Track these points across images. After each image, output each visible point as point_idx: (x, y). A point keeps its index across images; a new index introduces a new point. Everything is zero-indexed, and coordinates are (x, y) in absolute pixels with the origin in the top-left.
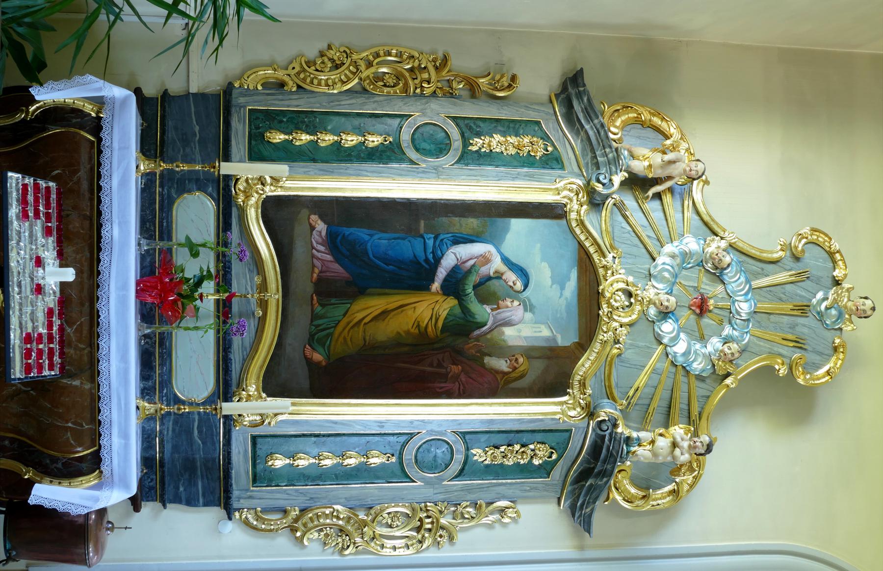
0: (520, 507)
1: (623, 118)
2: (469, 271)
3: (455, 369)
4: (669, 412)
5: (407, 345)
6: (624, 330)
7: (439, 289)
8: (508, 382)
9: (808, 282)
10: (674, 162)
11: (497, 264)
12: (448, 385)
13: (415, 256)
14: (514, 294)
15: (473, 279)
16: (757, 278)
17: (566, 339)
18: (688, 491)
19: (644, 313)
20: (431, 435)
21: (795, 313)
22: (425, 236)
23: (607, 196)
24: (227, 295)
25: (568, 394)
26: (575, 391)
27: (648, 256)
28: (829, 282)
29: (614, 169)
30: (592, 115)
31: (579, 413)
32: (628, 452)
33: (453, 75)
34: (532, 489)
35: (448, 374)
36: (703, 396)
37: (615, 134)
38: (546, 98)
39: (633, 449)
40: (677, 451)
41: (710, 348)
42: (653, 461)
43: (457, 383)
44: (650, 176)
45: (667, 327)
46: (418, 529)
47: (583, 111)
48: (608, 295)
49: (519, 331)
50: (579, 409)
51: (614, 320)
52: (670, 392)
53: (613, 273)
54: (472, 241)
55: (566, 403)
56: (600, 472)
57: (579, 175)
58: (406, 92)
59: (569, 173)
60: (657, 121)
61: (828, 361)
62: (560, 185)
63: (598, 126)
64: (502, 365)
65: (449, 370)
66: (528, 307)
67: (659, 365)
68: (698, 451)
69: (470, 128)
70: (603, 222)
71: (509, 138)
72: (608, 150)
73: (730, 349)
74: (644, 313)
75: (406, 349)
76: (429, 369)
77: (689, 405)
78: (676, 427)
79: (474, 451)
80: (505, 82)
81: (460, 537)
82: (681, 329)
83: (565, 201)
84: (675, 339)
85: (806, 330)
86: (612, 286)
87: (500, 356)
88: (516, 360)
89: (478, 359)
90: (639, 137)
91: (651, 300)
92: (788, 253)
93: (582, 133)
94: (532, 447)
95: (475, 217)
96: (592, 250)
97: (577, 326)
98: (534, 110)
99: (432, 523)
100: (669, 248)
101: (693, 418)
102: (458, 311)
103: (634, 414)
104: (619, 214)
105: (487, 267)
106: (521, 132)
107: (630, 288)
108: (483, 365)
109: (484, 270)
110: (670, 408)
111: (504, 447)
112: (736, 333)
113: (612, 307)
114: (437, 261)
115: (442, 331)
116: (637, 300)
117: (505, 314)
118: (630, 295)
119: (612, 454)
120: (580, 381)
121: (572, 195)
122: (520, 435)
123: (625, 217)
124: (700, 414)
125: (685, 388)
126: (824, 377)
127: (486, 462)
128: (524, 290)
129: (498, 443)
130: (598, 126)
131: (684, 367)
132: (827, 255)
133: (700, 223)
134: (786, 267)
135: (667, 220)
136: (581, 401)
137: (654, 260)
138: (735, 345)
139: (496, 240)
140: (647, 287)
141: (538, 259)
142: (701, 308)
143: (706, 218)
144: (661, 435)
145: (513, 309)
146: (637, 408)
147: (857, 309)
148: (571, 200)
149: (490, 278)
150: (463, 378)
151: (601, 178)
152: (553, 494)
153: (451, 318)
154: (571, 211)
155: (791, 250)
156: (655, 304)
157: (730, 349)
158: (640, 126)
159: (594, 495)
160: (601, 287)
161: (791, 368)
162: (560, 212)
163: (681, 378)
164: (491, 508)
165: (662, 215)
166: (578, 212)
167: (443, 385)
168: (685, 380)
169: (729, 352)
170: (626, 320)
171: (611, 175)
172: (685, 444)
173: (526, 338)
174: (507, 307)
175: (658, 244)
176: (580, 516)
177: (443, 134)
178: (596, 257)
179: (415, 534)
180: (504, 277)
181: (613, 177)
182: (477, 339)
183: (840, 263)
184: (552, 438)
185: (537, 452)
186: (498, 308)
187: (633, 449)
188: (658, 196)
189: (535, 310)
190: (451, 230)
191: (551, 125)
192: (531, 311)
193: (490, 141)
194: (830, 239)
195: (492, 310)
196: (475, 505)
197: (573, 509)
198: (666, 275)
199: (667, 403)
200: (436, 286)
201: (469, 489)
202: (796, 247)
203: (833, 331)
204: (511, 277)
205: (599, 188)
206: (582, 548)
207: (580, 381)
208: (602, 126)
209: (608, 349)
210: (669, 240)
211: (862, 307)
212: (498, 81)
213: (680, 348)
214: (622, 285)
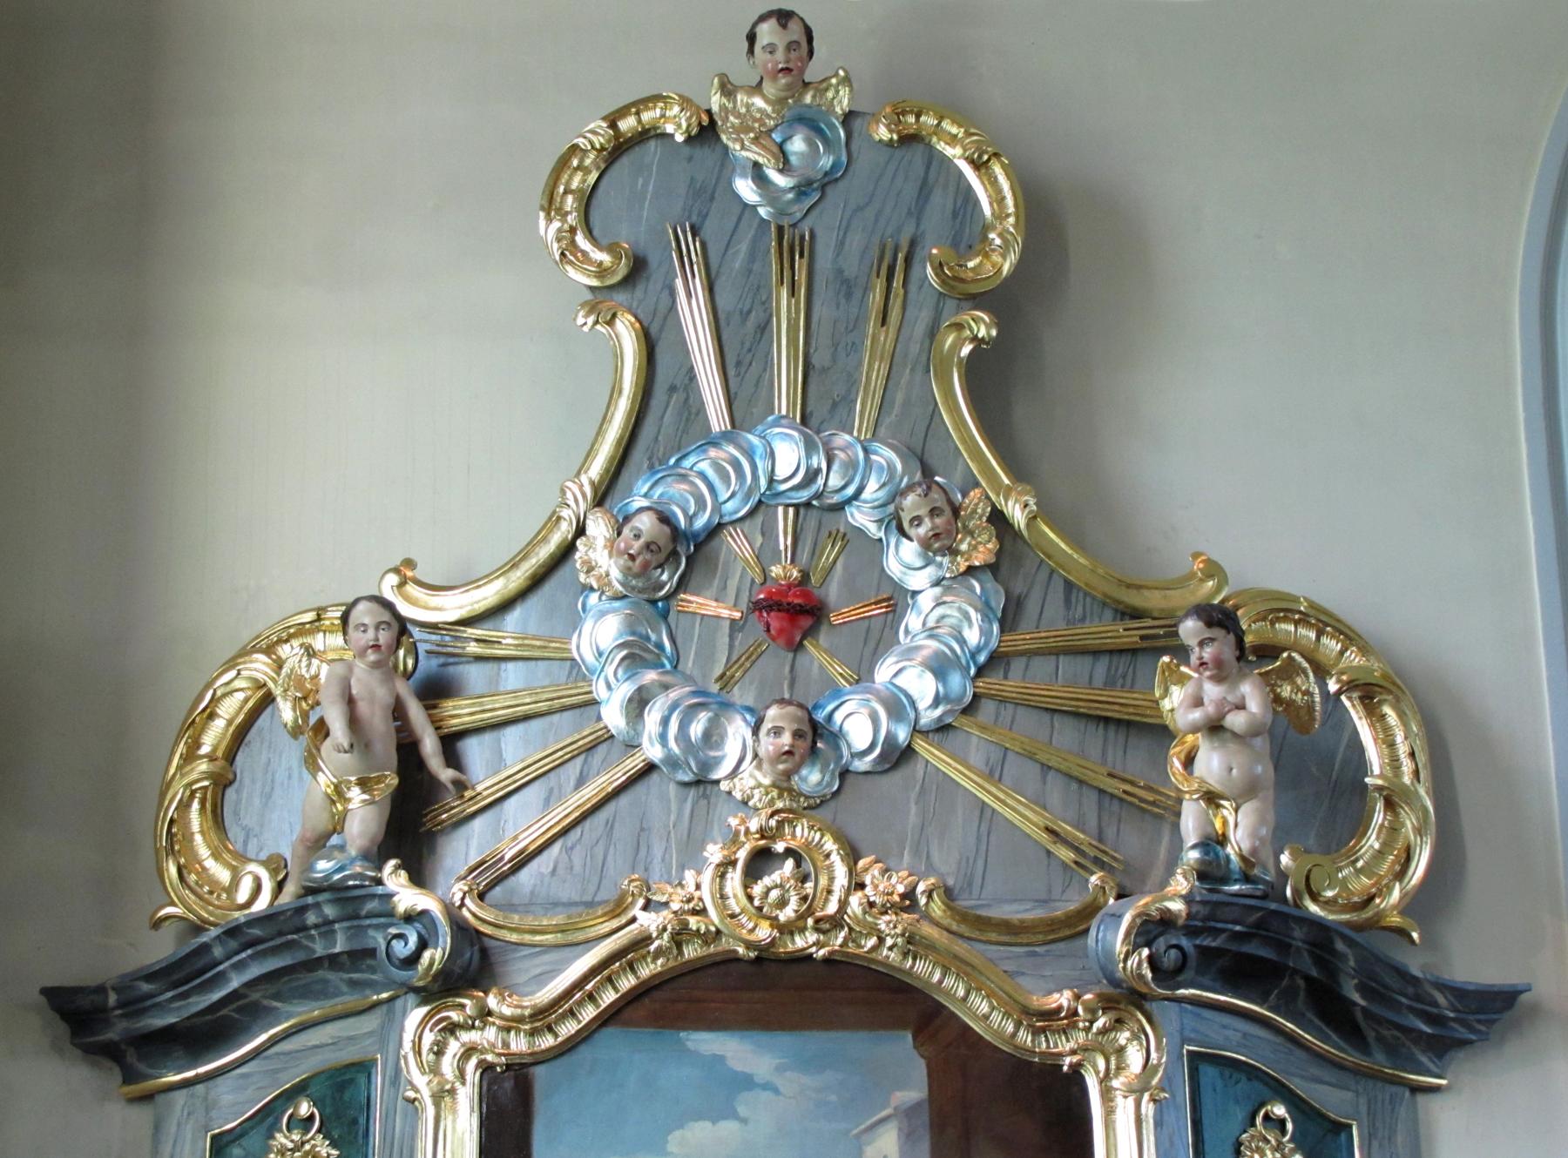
1: (204, 852)
4: (1119, 722)
9: (708, 231)
10: (350, 702)
16: (701, 409)
18: (1364, 650)
19: (815, 805)
21: (801, 277)
25: (1076, 1069)
27: (639, 789)
28: (704, 154)
29: (371, 906)
30: (200, 964)
31: (1135, 1037)
32: (1247, 878)
36: (1067, 601)
37: (258, 889)
40: (1236, 721)
41: (918, 580)
42: (1271, 793)
44: (393, 781)
45: (858, 726)
48: (764, 932)
50: (1123, 1037)
52: (1056, 717)
53: (695, 912)
55: (1105, 1080)
56: (1320, 962)
57: (391, 1012)
59: (383, 1048)
60: (214, 736)
61: (946, 162)
62: (422, 1083)
67: (976, 758)
68: (1229, 653)
72: (311, 918)
74: (815, 805)
77: (1096, 653)
78: (1166, 704)
82: (862, 676)
84: (897, 705)
85: (855, 241)
92: (621, 297)
93: (255, 996)
96: (627, 983)
97: (862, 1035)
101: (1132, 639)
103: (1130, 841)
104: (512, 880)
107: (742, 855)
110: (1107, 720)
112: (872, 490)
113: (801, 917)
118: (761, 861)
119: (1259, 925)
120: (1037, 1032)
121: (454, 1047)
123: (523, 860)
125: (1042, 666)
126: (994, 182)
131: (981, 671)
133: (535, 601)
134: (663, 308)
135: (526, 718)
136: (1099, 1024)
138: (910, 500)
140: (738, 795)
142: (795, 613)
143: (517, 579)
144: (1189, 762)
146: (1110, 832)
147: (787, 70)
148: (469, 1051)
151: (402, 950)
152: (1402, 1112)
155: (611, 287)
156: (788, 775)
157: (917, 521)
158: (230, 793)
159: (1391, 980)
162: (508, 1085)
163: (1011, 683)
165: (511, 733)
168: (1018, 665)
171: (390, 914)
172: (1212, 691)
175: (602, 749)
178: (646, 971)
181: (401, 909)
183: (647, 116)
188: (450, 743)
194: (575, 147)
198: (696, 729)
199: (1091, 727)
202: (602, 272)
203: (854, 147)
205: (434, 957)
207: (1037, 1032)
209: (927, 930)
210: (590, 710)
211: (780, 55)
213: (922, 687)
214: (735, 878)
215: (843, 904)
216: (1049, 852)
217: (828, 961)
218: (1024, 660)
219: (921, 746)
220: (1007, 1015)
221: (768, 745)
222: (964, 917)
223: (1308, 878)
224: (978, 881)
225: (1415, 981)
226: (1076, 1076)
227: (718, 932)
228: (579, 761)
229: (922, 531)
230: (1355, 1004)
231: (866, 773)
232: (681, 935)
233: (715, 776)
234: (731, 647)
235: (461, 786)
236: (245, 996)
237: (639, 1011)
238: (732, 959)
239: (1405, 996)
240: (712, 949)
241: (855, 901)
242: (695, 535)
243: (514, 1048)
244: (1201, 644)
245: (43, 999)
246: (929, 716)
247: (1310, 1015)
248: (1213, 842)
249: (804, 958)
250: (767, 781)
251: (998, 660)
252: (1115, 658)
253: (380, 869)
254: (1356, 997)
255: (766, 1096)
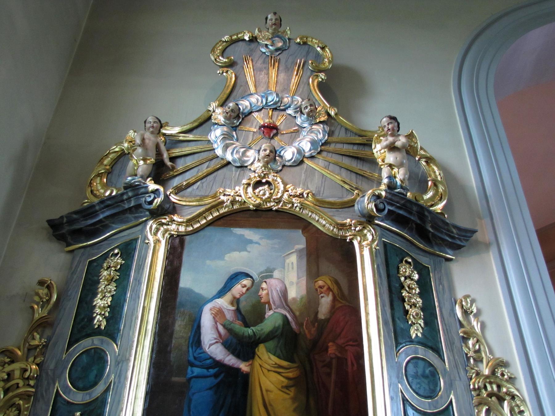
0: (460, 294)
2: (230, 330)
3: (332, 349)
5: (308, 401)
6: (290, 187)
7: (247, 364)
8: (343, 296)
11: (223, 303)
12: (350, 357)
13: (210, 389)
14: (255, 287)
15: (238, 327)
17: (300, 241)
20: (402, 378)
22: (189, 375)
23: (167, 197)
24: (313, 127)
25: (351, 240)
26: (349, 235)
27: (225, 170)
30: (91, 211)
33: (24, 344)
34: (441, 283)
35: (338, 358)
36: (346, 133)
38: (69, 257)
39: (399, 183)
43: (347, 348)
45: (289, 154)
46: (501, 400)
47: (86, 220)
48: (258, 201)
49: (292, 283)
50: (365, 231)
51: (281, 197)
53: (238, 196)
54: (199, 327)
55: (360, 243)
56: (420, 219)
58: (29, 396)
62: (151, 238)
63: (102, 206)
64: (326, 301)
65: (333, 356)
66: (268, 274)
69: (83, 327)
70: (191, 204)
71: (100, 290)
73: (306, 107)
75: (312, 403)
76: (333, 377)
78: (374, 151)
79: (414, 336)
80: (43, 291)
81: (499, 354)
83: (167, 235)
86: (251, 198)
87: (317, 304)
88: (321, 287)
89: (322, 326)
90: (119, 176)
91: (264, 166)
93: (107, 222)
94: (402, 279)
95: (173, 324)
96: (216, 214)
98: (77, 266)
99: (491, 383)
100: (219, 152)
102: (271, 344)
104: (184, 192)
105: (226, 313)
106: (96, 278)
107: (252, 182)
108: (327, 320)
109: (229, 316)
111: (406, 305)
114: (218, 364)
115: (291, 360)
116: (264, 177)
117: (275, 296)
118: (258, 184)
119: (404, 205)
120: (339, 230)
121: (162, 229)
122: (393, 289)
124: (360, 136)
127: (422, 325)
128: (251, 277)
129: (402, 312)
130: (102, 206)
132: (233, 45)
137: (229, 163)
139: (199, 304)
141: (220, 263)
142: (270, 130)
143: (196, 124)
144: (383, 161)
145: (270, 289)
147: (275, 24)
149: (238, 311)
150: (340, 341)
151: (149, 199)
153: (279, 351)
154: (178, 231)
157: (306, 107)
159: (441, 224)
160: (251, 207)
161: (320, 71)
162: (177, 241)
163: (332, 147)
164: (465, 323)
166: (180, 224)
167: (349, 363)
169: (309, 107)
170: (281, 187)
173: (298, 278)
174: (268, 294)
176: (460, 240)
177: (84, 356)
178: (222, 211)
179: (506, 402)
180: (238, 296)
182: (300, 325)
183: (239, 36)
184: (394, 259)
185: (407, 274)
186: (269, 303)
187: (399, 183)
189: (271, 267)
190: (185, 348)
191: (96, 251)
192: (272, 272)
193: (99, 307)
195: (270, 309)
196: (465, 339)
197: (456, 248)
199: (353, 160)
200: (244, 367)
201: (451, 344)
204: (237, 289)
206: (487, 246)
208: (102, 202)
210: (212, 152)
212: (41, 298)
214: (250, 189)
215: (281, 197)
216: (342, 186)
217: (277, 211)
218: (334, 144)
219: (305, 160)
220: (331, 225)
221: (262, 154)
222: (318, 201)
223: (415, 198)
224: (322, 192)
225: (447, 224)
226: (351, 243)
227: (245, 202)
228: (208, 163)
229: (307, 110)
230: (430, 232)
231: (290, 166)
232: (233, 202)
233: (246, 165)
234: (253, 137)
235: (173, 168)
236: (104, 222)
237: (219, 223)
238: (249, 210)
239: (444, 229)
240: (242, 206)
241: (286, 196)
242: (245, 113)
243: (180, 230)
244: (388, 124)
245: (46, 225)
246: (307, 154)
247: (416, 236)
248: (391, 177)
249: (270, 210)
250: (261, 165)
251: (326, 143)
252: (359, 146)
253: (146, 180)
254: (430, 229)
255: (257, 245)
